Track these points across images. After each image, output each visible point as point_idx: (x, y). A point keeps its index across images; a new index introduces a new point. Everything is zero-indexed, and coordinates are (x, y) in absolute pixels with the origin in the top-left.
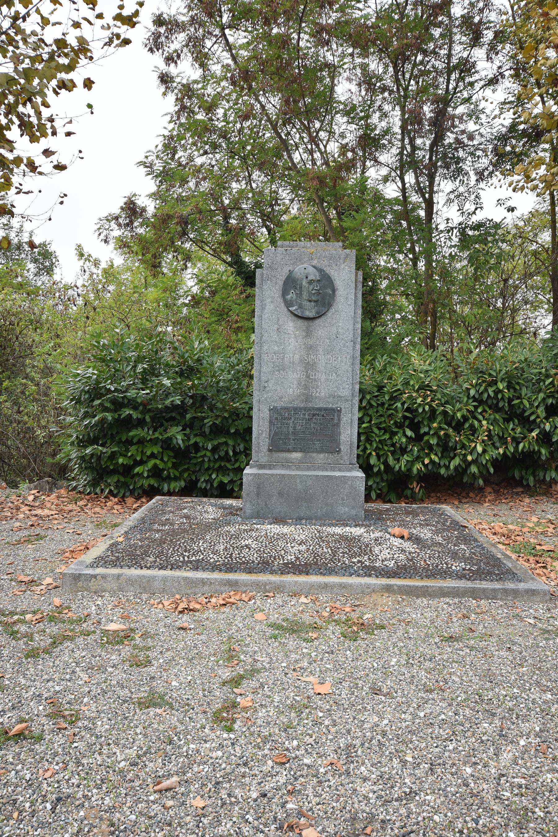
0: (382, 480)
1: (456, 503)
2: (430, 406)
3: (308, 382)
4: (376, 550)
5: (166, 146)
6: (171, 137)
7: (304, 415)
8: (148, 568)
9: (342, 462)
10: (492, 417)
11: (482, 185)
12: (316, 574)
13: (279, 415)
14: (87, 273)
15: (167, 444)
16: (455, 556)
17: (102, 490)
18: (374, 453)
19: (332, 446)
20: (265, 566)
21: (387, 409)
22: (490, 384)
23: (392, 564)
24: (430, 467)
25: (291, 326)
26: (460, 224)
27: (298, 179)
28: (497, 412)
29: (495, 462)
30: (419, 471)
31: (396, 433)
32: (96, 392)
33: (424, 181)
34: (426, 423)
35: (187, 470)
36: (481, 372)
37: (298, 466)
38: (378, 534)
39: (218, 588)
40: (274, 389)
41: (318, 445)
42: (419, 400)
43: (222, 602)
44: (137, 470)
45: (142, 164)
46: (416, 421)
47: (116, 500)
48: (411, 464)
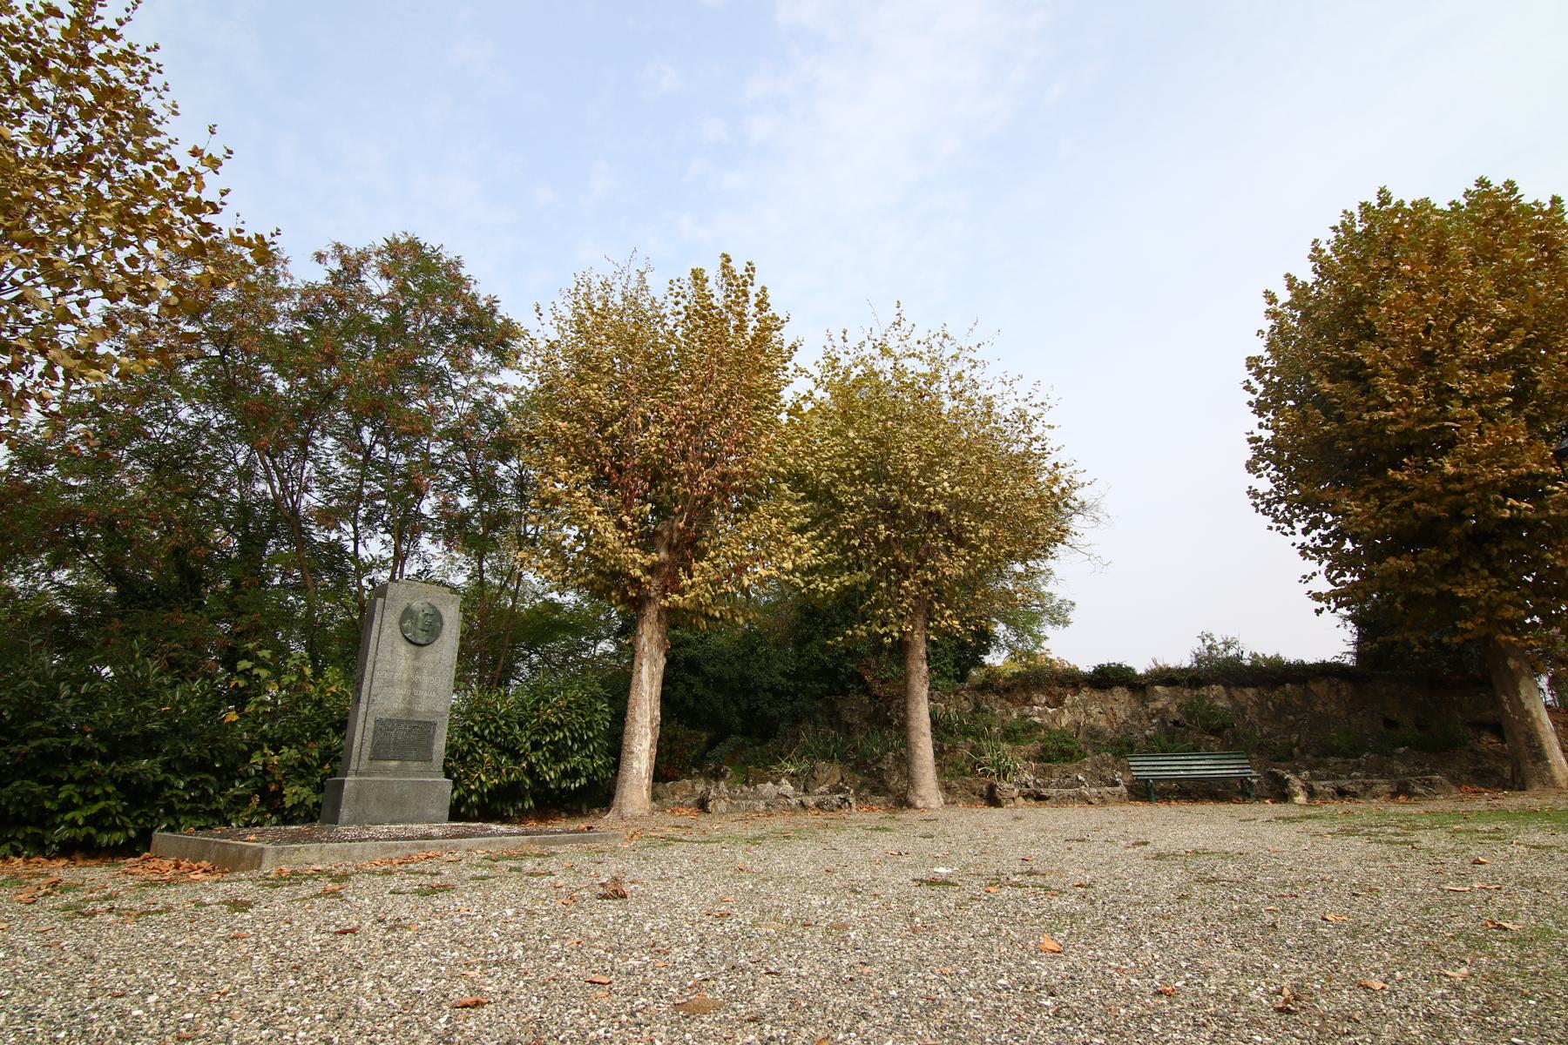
3: (412, 699)
25: (403, 649)
37: (395, 772)
41: (414, 754)
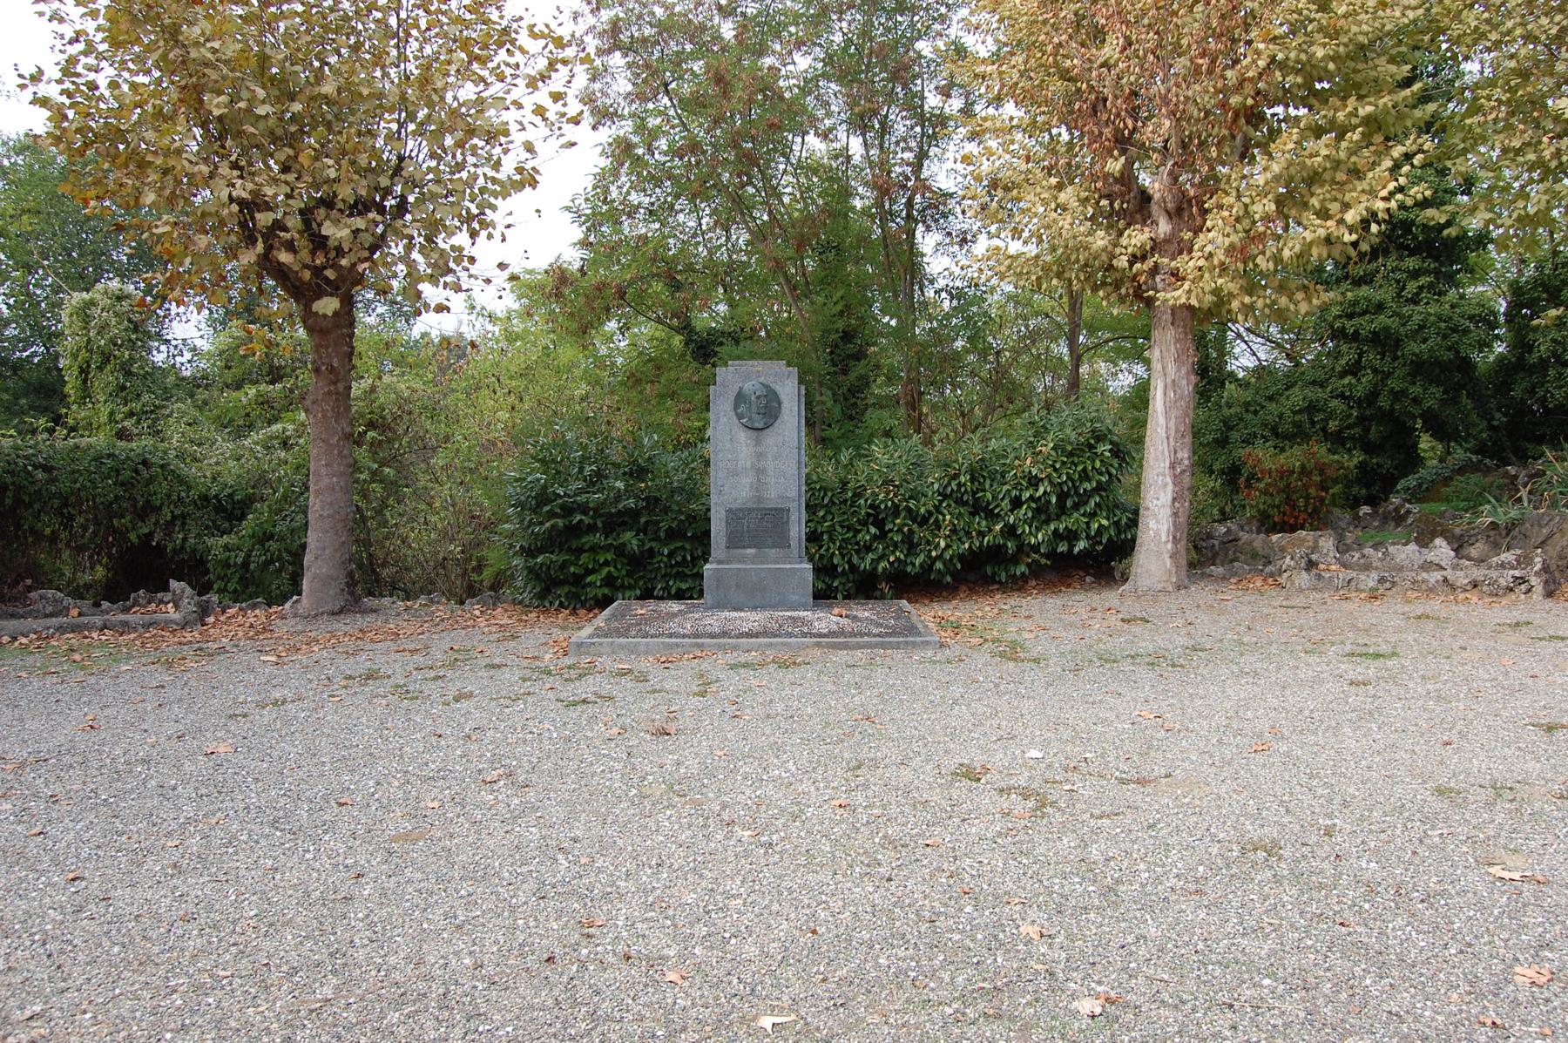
3: (759, 485)
13: (734, 515)
15: (620, 550)
19: (782, 542)
20: (724, 634)
25: (742, 436)
30: (884, 569)
31: (859, 531)
32: (543, 497)
37: (753, 560)
44: (589, 579)
45: (568, 209)
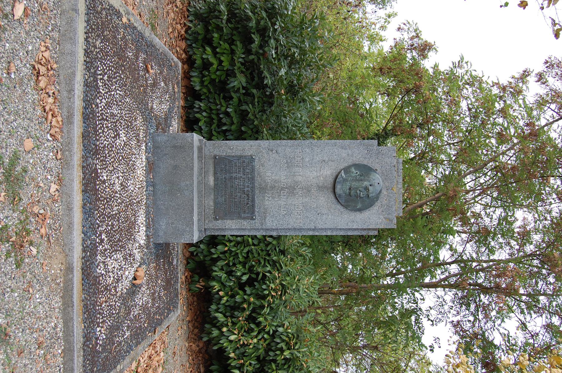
0: (205, 256)
1: (188, 319)
2: (268, 295)
3: (277, 189)
4: (119, 256)
5: (474, 78)
6: (481, 82)
7: (248, 187)
8: (86, 39)
9: (207, 221)
10: (261, 347)
11: (449, 325)
12: (83, 200)
13: (247, 163)
14: (376, 21)
15: (230, 74)
16: (114, 329)
17: (191, 21)
18: (226, 249)
19: (221, 212)
21: (265, 259)
22: (287, 344)
23: (101, 270)
24: (216, 296)
25: (328, 172)
26: (420, 309)
27: (452, 182)
28: (265, 350)
29: (222, 350)
31: (244, 267)
33: (453, 280)
34: (254, 291)
35: (210, 92)
36: (298, 336)
38: (138, 257)
39: (66, 105)
40: (270, 158)
41: (221, 199)
42: (272, 286)
43: (47, 108)
44: (208, 49)
45: (462, 58)
46: (255, 283)
47: (183, 32)
48: (219, 280)
